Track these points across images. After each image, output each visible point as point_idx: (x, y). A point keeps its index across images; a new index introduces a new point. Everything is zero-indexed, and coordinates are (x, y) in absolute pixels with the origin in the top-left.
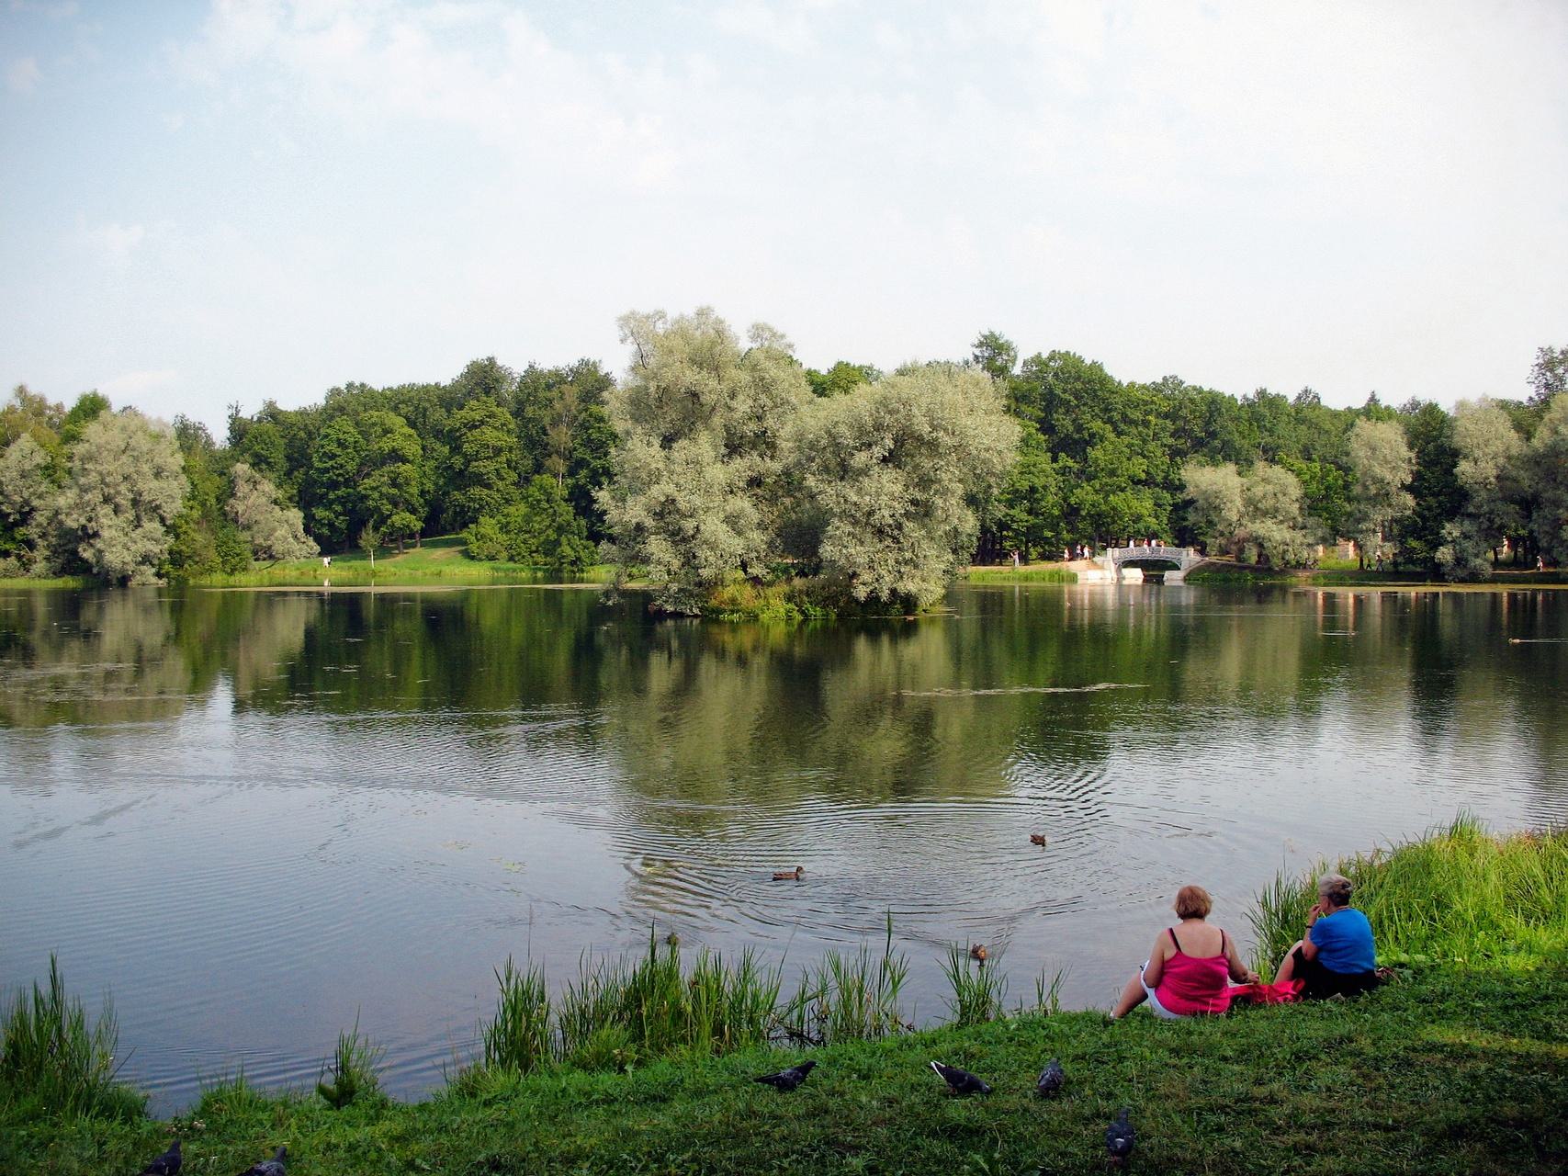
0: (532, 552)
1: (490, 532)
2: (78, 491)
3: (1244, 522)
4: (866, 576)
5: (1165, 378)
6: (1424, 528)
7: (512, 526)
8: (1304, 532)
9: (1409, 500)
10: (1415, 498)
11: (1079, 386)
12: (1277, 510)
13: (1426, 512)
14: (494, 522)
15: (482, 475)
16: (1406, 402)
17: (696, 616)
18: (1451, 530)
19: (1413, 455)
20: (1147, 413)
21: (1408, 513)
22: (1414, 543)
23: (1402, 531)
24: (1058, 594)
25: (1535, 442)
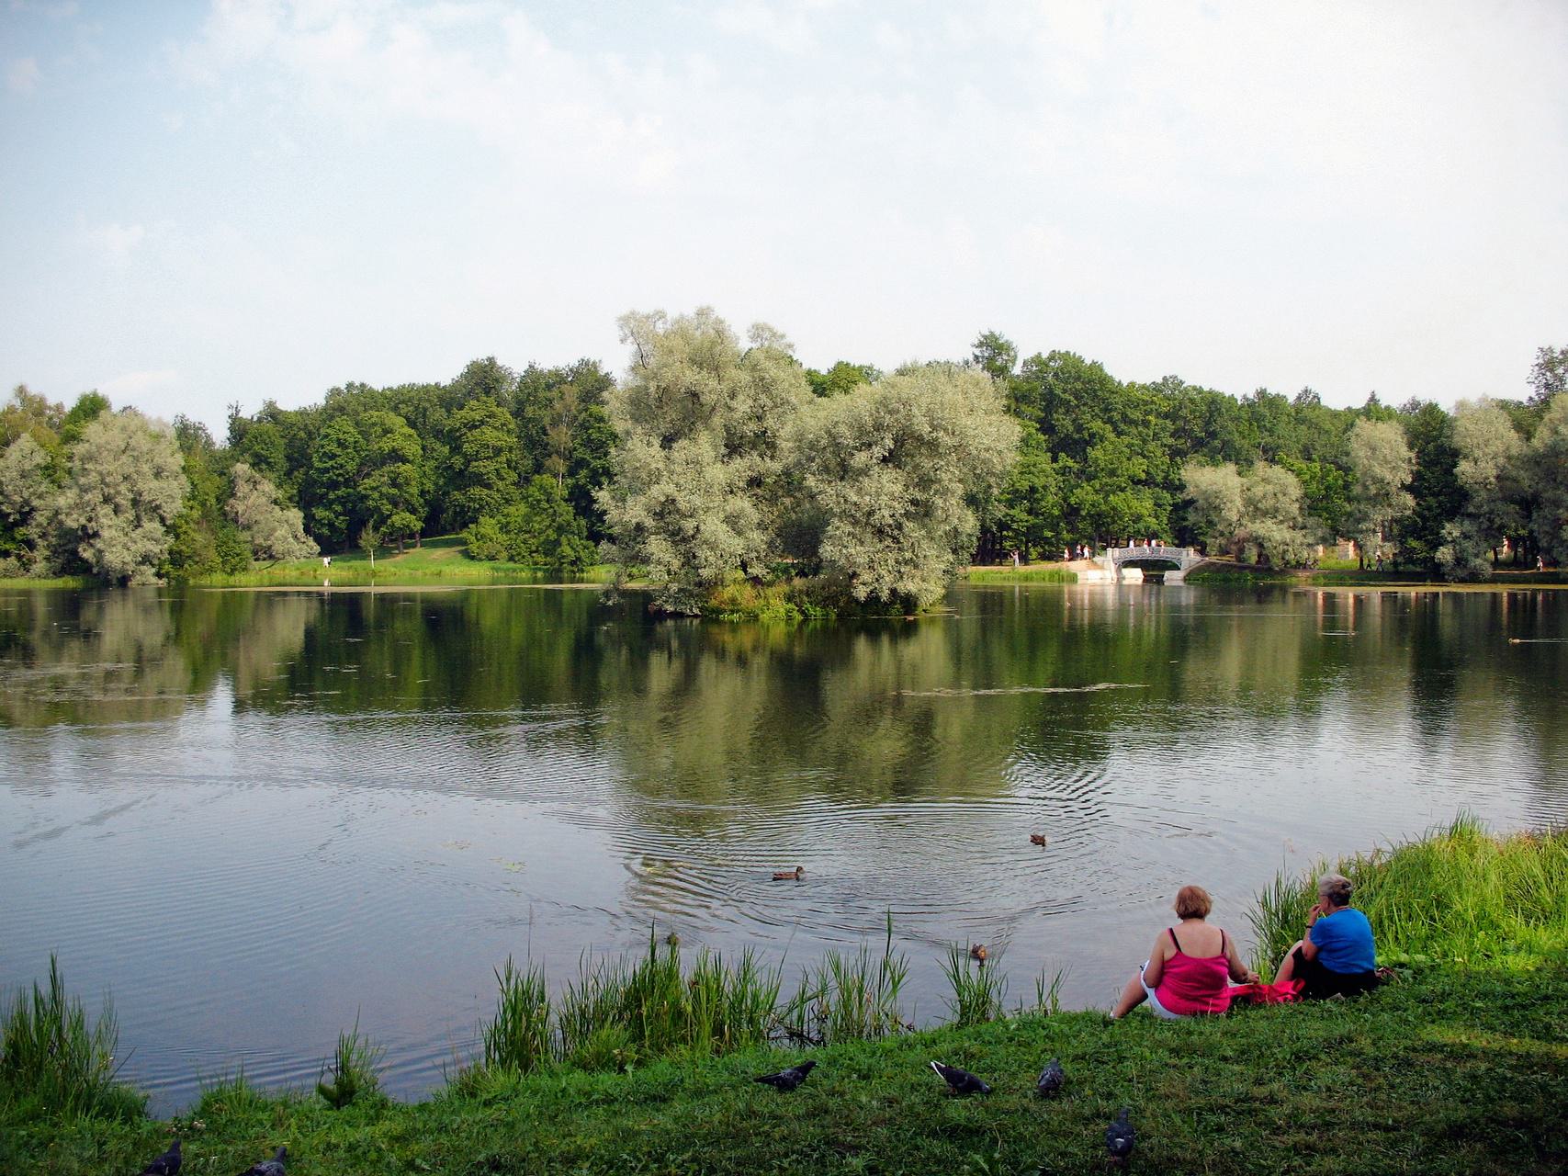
0: (531, 552)
1: (490, 532)
2: (78, 491)
3: (1244, 522)
4: (866, 576)
5: (1165, 378)
6: (1424, 528)
7: (512, 526)
8: (1304, 532)
9: (1409, 500)
10: (1415, 498)
11: (1079, 386)
12: (1277, 510)
13: (1426, 512)
14: (492, 520)
15: (482, 475)
16: (1406, 402)
17: (696, 616)
18: (1451, 530)
19: (1412, 455)
20: (1148, 413)
21: (1408, 513)
22: (1414, 543)
23: (1402, 531)
24: (1058, 594)
25: (1535, 442)
